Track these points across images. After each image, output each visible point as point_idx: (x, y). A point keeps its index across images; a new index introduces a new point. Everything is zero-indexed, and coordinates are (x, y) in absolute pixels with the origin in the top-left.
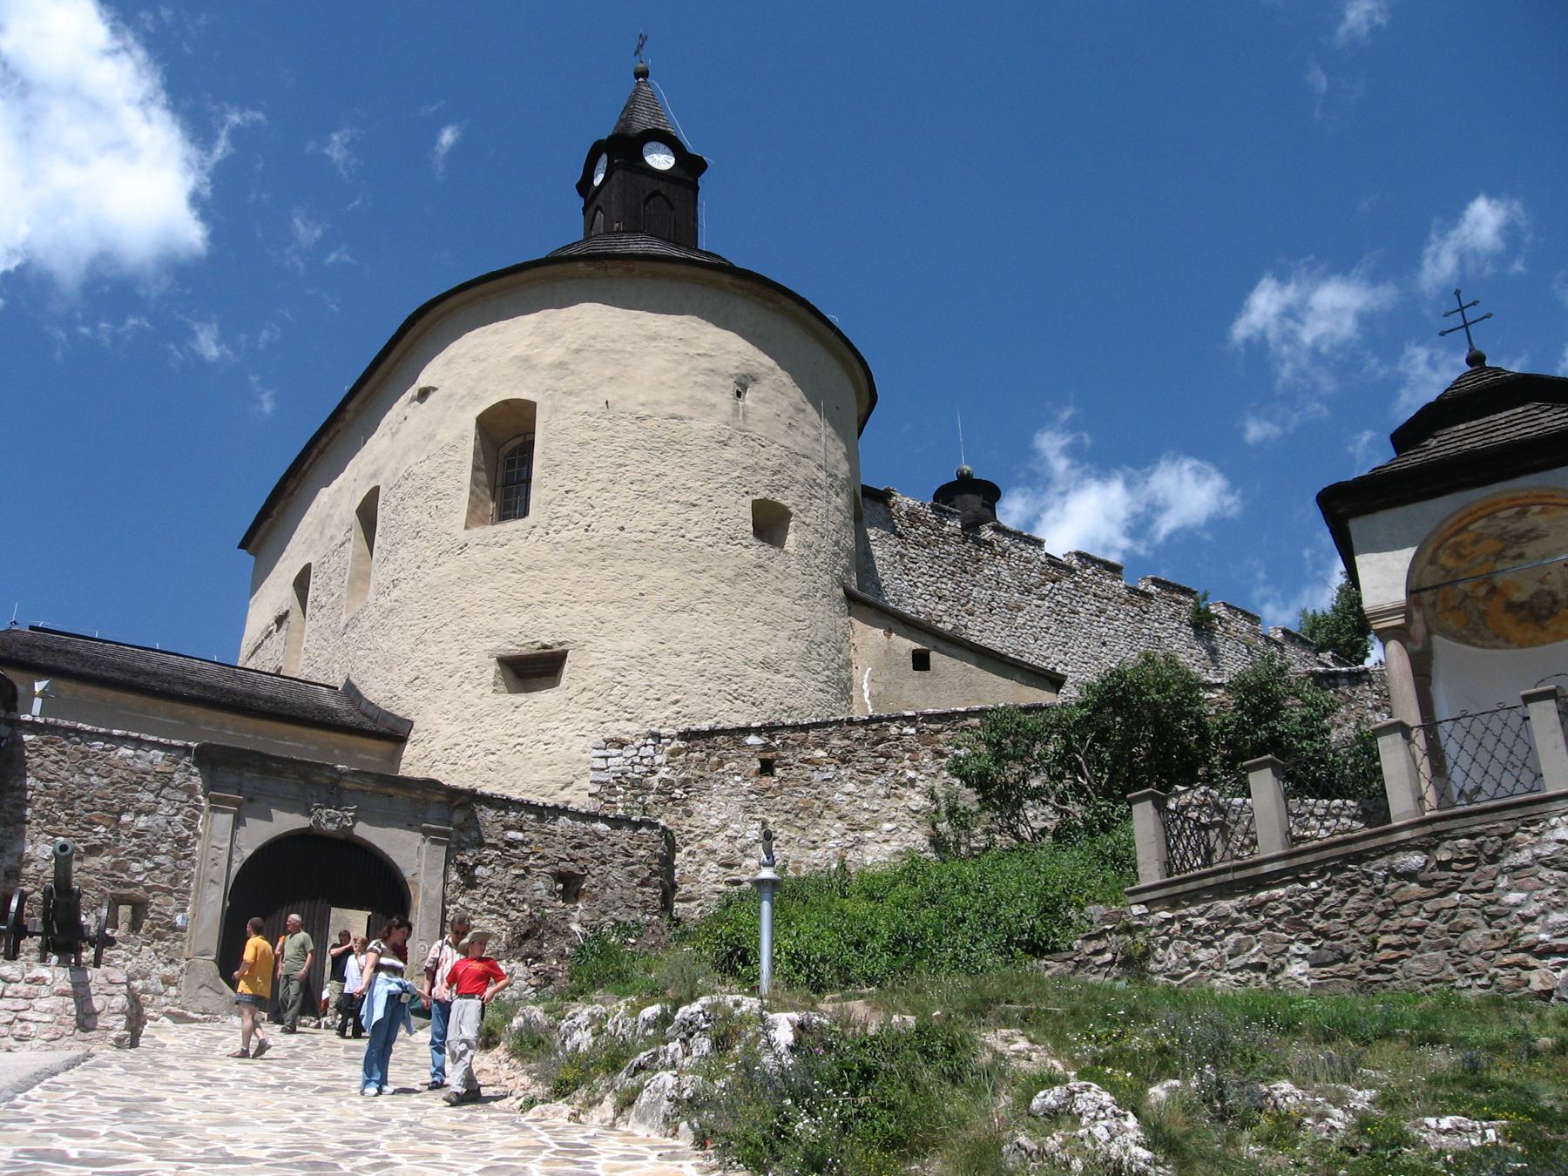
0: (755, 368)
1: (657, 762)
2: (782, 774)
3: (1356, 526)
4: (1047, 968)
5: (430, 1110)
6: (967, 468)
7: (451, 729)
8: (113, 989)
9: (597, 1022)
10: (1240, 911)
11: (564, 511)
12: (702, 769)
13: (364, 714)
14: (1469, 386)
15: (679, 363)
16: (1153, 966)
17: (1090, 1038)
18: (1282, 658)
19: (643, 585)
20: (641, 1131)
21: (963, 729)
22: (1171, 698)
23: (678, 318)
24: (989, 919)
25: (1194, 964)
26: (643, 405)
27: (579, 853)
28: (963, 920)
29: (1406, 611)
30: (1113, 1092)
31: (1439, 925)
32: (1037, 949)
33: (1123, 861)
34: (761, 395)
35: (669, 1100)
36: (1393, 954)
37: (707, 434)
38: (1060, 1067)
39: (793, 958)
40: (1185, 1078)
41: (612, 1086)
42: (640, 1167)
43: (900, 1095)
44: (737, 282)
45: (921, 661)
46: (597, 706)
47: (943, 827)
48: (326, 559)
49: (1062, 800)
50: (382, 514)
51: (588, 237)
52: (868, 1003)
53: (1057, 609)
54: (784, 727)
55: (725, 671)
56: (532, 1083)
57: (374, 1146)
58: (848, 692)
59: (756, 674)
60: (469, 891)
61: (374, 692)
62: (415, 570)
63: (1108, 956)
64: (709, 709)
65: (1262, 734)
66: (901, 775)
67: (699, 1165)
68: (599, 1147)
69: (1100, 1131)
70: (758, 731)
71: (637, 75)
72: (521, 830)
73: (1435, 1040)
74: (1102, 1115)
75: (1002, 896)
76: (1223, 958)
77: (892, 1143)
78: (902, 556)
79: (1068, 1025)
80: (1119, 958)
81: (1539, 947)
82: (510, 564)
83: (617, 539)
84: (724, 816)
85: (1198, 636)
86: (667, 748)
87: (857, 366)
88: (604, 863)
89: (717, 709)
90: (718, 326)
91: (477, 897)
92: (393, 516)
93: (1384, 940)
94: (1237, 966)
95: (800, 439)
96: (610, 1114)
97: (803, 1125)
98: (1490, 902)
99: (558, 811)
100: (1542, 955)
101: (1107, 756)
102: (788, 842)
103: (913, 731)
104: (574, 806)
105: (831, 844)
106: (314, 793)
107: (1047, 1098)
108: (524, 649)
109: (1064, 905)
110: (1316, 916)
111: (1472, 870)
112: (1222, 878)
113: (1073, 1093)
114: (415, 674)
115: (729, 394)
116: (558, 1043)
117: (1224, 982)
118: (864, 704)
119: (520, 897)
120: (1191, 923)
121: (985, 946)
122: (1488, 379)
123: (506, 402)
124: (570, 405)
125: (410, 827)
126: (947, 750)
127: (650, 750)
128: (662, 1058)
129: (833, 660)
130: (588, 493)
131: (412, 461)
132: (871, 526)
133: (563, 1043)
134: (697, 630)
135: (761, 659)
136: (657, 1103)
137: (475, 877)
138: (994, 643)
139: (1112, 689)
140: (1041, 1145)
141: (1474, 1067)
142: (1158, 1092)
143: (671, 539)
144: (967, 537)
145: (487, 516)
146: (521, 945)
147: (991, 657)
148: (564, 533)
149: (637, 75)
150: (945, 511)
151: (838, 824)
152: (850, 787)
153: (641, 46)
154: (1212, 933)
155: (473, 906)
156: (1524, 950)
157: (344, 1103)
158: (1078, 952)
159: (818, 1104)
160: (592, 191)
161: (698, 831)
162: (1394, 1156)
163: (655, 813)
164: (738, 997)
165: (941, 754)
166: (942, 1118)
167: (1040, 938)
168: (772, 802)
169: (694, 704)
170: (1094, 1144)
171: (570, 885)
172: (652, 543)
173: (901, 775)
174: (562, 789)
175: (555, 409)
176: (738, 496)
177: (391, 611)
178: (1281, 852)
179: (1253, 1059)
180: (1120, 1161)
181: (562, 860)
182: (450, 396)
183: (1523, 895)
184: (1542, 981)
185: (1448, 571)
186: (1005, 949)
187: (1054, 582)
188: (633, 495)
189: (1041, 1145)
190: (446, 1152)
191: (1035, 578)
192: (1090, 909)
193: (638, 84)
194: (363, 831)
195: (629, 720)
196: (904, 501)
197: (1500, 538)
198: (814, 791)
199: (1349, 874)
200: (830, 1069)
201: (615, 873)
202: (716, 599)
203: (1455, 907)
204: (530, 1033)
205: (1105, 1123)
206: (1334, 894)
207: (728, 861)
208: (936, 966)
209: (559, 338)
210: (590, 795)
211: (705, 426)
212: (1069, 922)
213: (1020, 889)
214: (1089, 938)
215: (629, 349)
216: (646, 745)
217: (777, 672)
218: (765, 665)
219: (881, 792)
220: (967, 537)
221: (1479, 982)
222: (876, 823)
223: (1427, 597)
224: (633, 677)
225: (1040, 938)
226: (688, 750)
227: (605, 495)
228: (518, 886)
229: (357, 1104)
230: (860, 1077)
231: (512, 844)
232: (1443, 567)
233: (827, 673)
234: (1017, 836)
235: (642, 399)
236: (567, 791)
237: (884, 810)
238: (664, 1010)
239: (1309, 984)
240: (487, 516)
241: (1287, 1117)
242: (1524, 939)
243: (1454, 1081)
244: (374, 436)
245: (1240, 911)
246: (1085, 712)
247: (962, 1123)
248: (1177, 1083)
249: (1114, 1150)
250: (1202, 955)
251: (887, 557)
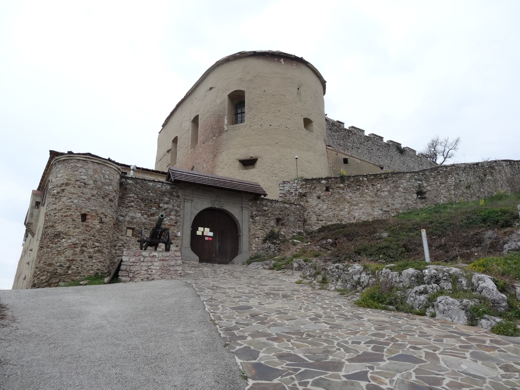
2: (332, 191)
8: (177, 258)
18: (421, 162)
26: (274, 92)
46: (267, 173)
84: (317, 202)
91: (257, 225)
102: (334, 209)
105: (346, 210)
115: (296, 90)
143: (284, 128)
148: (255, 127)
152: (350, 194)
161: (310, 206)
195: (275, 177)
198: (341, 196)
210: (280, 197)
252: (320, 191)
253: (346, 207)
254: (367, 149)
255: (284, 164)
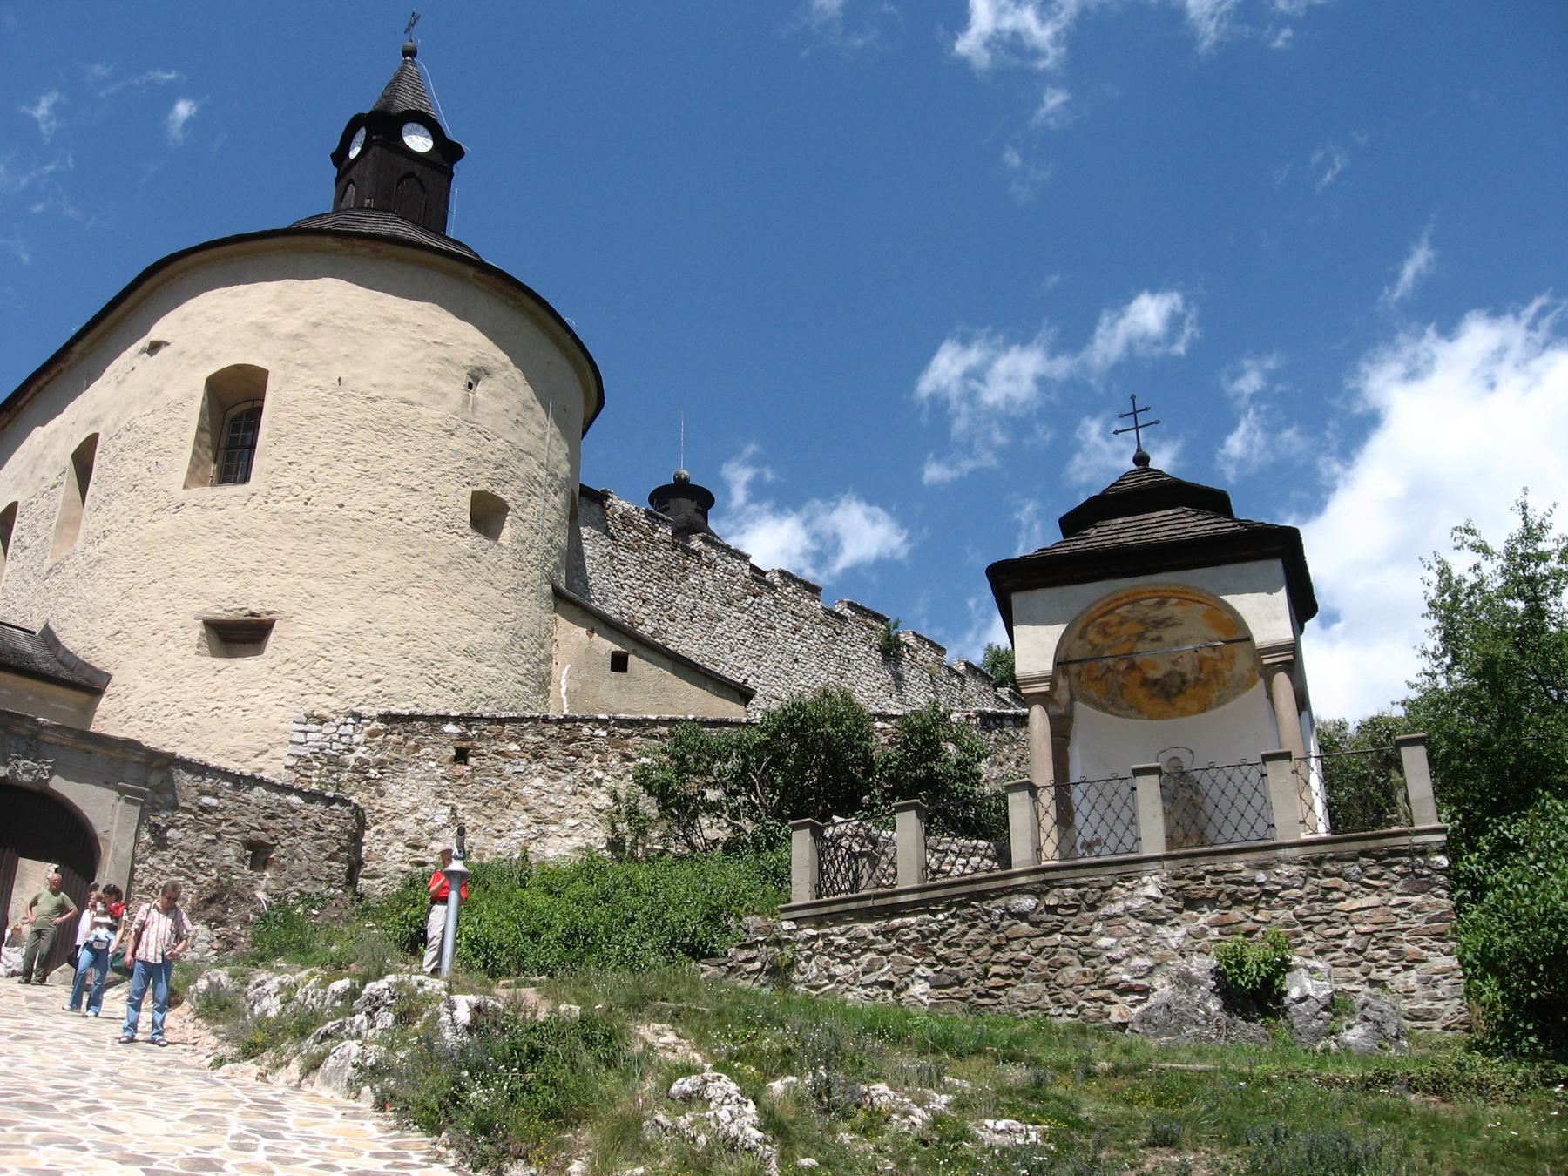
0: (488, 362)
1: (355, 741)
2: (476, 764)
3: (1017, 599)
4: (703, 970)
5: (126, 1063)
6: (685, 473)
7: (150, 687)
9: (287, 993)
10: (876, 934)
11: (285, 482)
12: (399, 752)
13: (61, 662)
14: (1130, 484)
15: (415, 349)
16: (796, 976)
17: (727, 1037)
18: (962, 690)
19: (357, 563)
20: (326, 1092)
21: (652, 736)
22: (843, 732)
23: (419, 304)
24: (656, 922)
25: (832, 977)
26: (375, 386)
27: (271, 823)
28: (633, 920)
29: (1052, 680)
30: (739, 1083)
31: (1041, 960)
32: (697, 952)
33: (781, 877)
34: (492, 389)
35: (354, 1066)
36: (1001, 982)
37: (434, 422)
38: (699, 1059)
39: (473, 943)
40: (801, 1076)
41: (299, 1051)
42: (326, 1123)
43: (561, 1074)
44: (481, 276)
45: (619, 663)
46: (300, 678)
47: (623, 827)
48: (34, 500)
49: (735, 815)
50: (99, 461)
51: (337, 210)
52: (538, 991)
53: (755, 623)
54: (481, 718)
55: (428, 655)
56: (219, 1044)
57: (83, 1091)
58: (546, 686)
59: (459, 661)
60: (159, 852)
61: (74, 640)
62: (128, 523)
63: (758, 965)
64: (409, 691)
65: (921, 772)
66: (589, 774)
67: (379, 1125)
68: (288, 1104)
69: (724, 1114)
70: (456, 720)
71: (405, 53)
72: (216, 796)
73: (1013, 1058)
74: (727, 1101)
75: (670, 902)
76: (857, 974)
77: (551, 1114)
78: (612, 557)
79: (713, 1024)
80: (767, 967)
81: (1121, 986)
82: (225, 528)
83: (335, 515)
84: (416, 799)
85: (885, 661)
86: (366, 729)
87: (587, 366)
88: (294, 835)
89: (417, 692)
90: (458, 316)
91: (167, 858)
92: (110, 466)
93: (994, 969)
94: (868, 982)
95: (525, 436)
96: (297, 1076)
97: (476, 1095)
98: (1086, 944)
99: (254, 781)
100: (1122, 992)
101: (779, 779)
103: (604, 733)
104: (266, 775)
105: (515, 834)
106: (12, 742)
107: (684, 1085)
108: (231, 614)
109: (725, 914)
110: (940, 944)
111: (1074, 915)
112: (863, 904)
113: (706, 1082)
114: (117, 627)
115: (461, 384)
116: (247, 1007)
117: (855, 996)
118: (560, 704)
119: (209, 861)
120: (832, 942)
121: (650, 946)
122: (1147, 480)
123: (238, 367)
124: (302, 377)
125: (106, 784)
126: (634, 755)
127: (350, 729)
128: (348, 1028)
129: (534, 654)
130: (311, 467)
131: (135, 413)
132: (586, 525)
133: (252, 1008)
134: (405, 612)
135: (465, 647)
136: (342, 1068)
137: (167, 839)
138: (691, 649)
139: (791, 720)
140: (674, 1123)
141: (1039, 1083)
142: (777, 1086)
143: (389, 521)
144: (676, 545)
145: (207, 477)
146: (205, 908)
147: (687, 666)
148: (284, 505)
149: (405, 53)
150: (658, 518)
151: (525, 816)
152: (539, 781)
153: (412, 25)
154: (850, 952)
155: (162, 867)
156: (1109, 987)
157: (42, 1051)
158: (732, 959)
159: (492, 1076)
160: (346, 163)
161: (388, 811)
162: (956, 1148)
163: (348, 791)
164: (422, 977)
165: (628, 758)
166: (595, 1096)
167: (700, 942)
168: (463, 790)
169: (395, 686)
170: (718, 1124)
171: (259, 854)
172: (369, 523)
173: (589, 774)
174: (256, 756)
175: (288, 380)
176: (459, 486)
177: (99, 561)
178: (916, 885)
179: (861, 1064)
180: (737, 1139)
181: (253, 828)
182: (182, 353)
183: (1113, 940)
184: (1120, 1015)
185: (1094, 646)
186: (667, 951)
187: (755, 596)
188: (355, 473)
189: (674, 1123)
190: (151, 1101)
191: (737, 591)
192: (748, 919)
193: (406, 62)
194: (59, 785)
195: (330, 694)
196: (620, 504)
197: (1141, 622)
198: (504, 783)
199: (971, 910)
200: (503, 1048)
201: (304, 845)
202: (428, 584)
203: (1056, 946)
204: (217, 996)
205: (729, 1108)
206: (957, 926)
207: (415, 843)
208: (604, 961)
209: (299, 309)
210: (287, 767)
211: (433, 414)
212: (727, 930)
213: (687, 896)
214: (742, 947)
215: (366, 329)
216: (345, 724)
217: (479, 661)
218: (468, 653)
219: (569, 789)
220: (676, 545)
221: (1069, 1011)
222: (560, 818)
223: (1074, 668)
224: (338, 652)
225: (700, 942)
226: (388, 733)
227: (328, 471)
228: (208, 851)
229: (54, 1053)
230: (528, 1057)
231: (206, 809)
232: (1090, 642)
233: (527, 666)
234: (691, 845)
235: (375, 380)
236: (260, 758)
237: (570, 806)
238: (353, 984)
239: (928, 1002)
240: (207, 477)
241: (879, 1113)
242: (1110, 978)
243: (1018, 1092)
244: (98, 382)
245: (876, 934)
246: (764, 737)
247: (612, 1101)
248: (794, 1079)
249: (734, 1130)
250: (839, 970)
251: (597, 557)
252: (434, 759)
253: (519, 824)
254: (751, 625)
255: (369, 651)
